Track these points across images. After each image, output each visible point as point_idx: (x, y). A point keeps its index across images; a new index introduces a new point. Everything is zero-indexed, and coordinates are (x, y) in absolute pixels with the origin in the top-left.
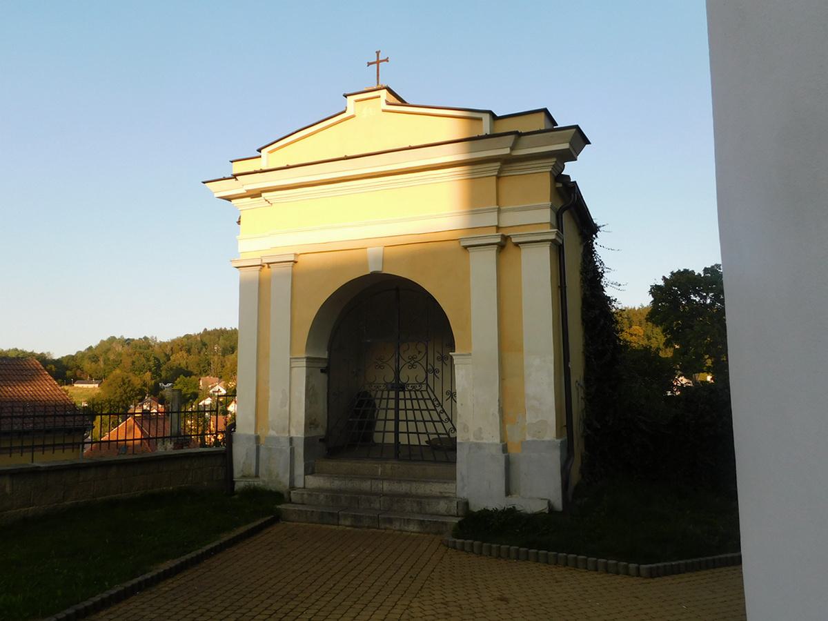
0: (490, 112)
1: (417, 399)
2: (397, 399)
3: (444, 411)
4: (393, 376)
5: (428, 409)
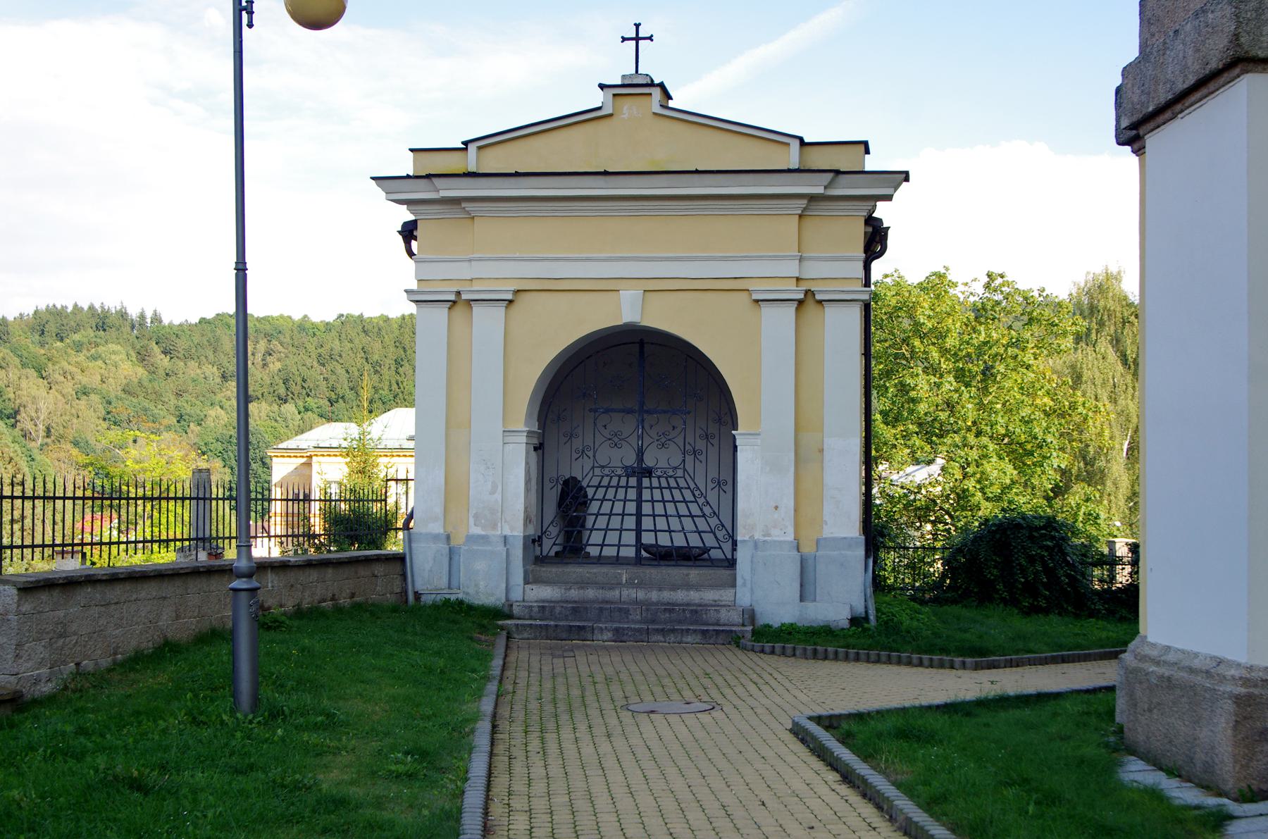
0: (801, 139)
1: (670, 488)
2: (640, 488)
3: (708, 503)
4: (634, 457)
5: (685, 501)
